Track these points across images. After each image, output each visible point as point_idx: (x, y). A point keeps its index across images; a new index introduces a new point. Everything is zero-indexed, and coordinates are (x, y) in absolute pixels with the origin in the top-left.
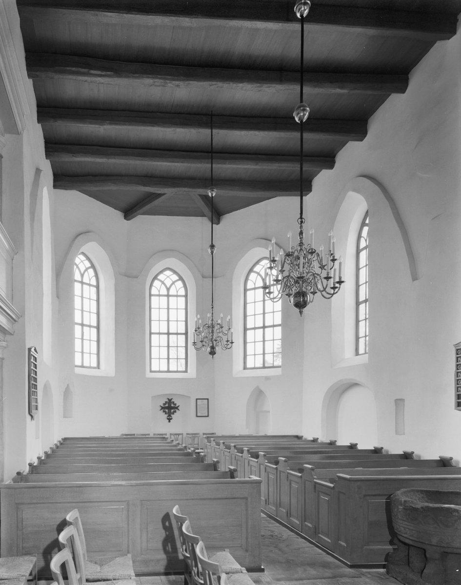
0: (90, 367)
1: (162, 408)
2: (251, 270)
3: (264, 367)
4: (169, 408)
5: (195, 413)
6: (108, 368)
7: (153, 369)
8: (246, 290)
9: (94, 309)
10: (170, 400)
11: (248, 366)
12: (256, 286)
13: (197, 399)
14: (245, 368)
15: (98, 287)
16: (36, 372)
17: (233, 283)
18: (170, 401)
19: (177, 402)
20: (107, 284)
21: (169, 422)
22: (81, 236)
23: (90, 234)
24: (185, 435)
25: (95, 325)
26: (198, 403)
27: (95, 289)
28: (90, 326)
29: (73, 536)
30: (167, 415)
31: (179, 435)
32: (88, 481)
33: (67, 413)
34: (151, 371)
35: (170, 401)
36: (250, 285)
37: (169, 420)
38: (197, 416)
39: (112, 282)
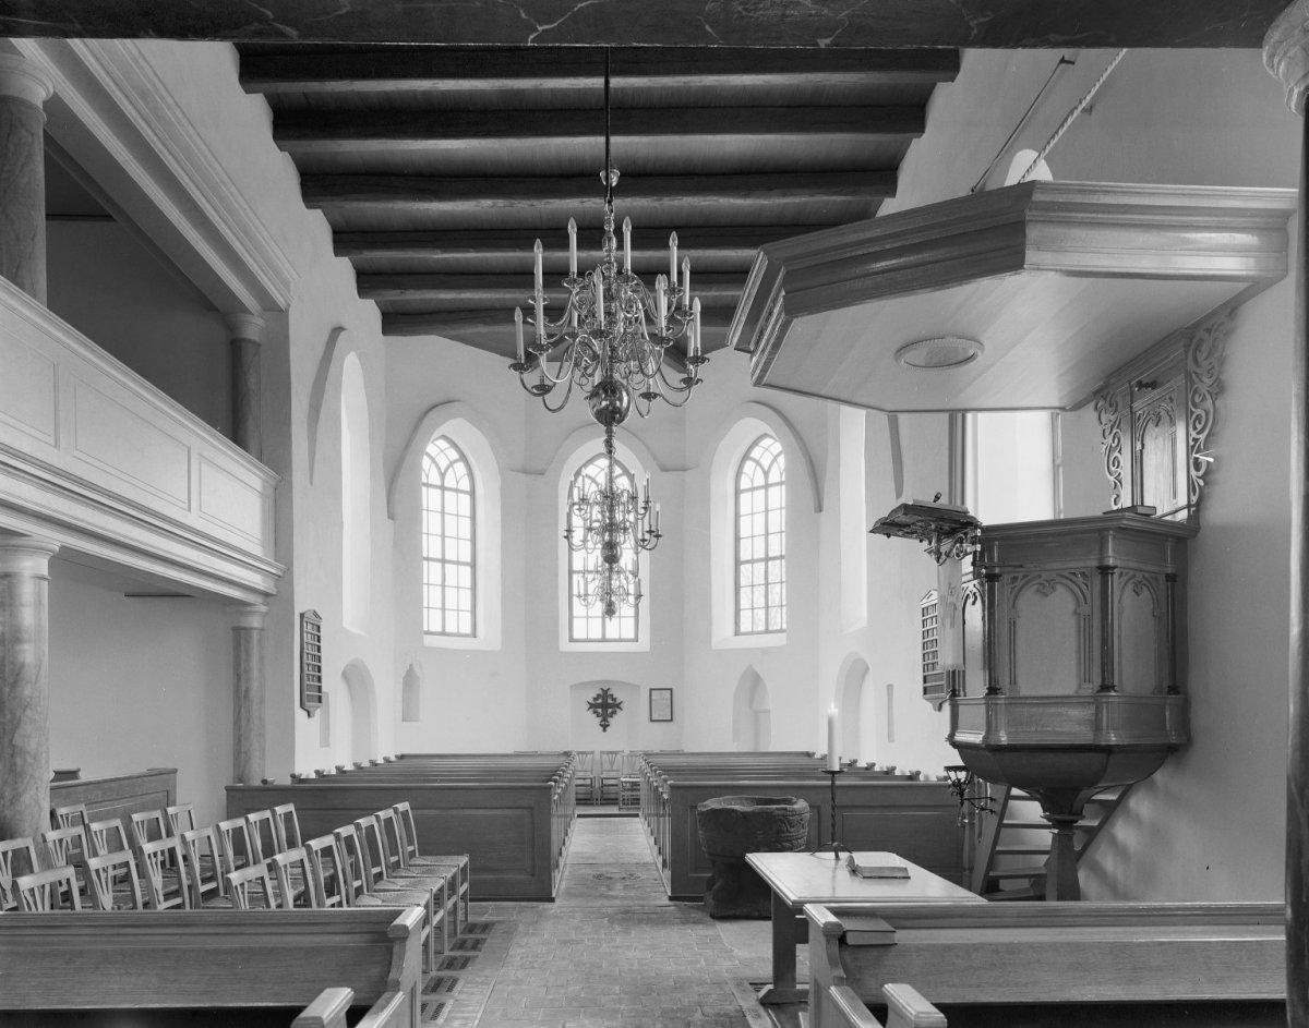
0: (458, 635)
1: (592, 706)
2: (746, 457)
3: (767, 631)
4: (605, 706)
5: (648, 716)
6: (490, 636)
7: (576, 636)
8: (737, 492)
9: (466, 532)
10: (605, 692)
11: (742, 630)
12: (755, 485)
13: (651, 690)
14: (737, 633)
15: (472, 493)
16: (319, 637)
17: (712, 477)
18: (605, 694)
19: (619, 695)
20: (489, 488)
21: (605, 730)
22: (436, 409)
23: (456, 403)
24: (597, 754)
25: (468, 560)
26: (653, 697)
27: (468, 497)
28: (458, 563)
29: (174, 848)
30: (599, 719)
31: (616, 753)
32: (416, 829)
33: (408, 714)
34: (572, 640)
35: (605, 694)
36: (745, 483)
37: (605, 727)
38: (651, 720)
39: (497, 485)
